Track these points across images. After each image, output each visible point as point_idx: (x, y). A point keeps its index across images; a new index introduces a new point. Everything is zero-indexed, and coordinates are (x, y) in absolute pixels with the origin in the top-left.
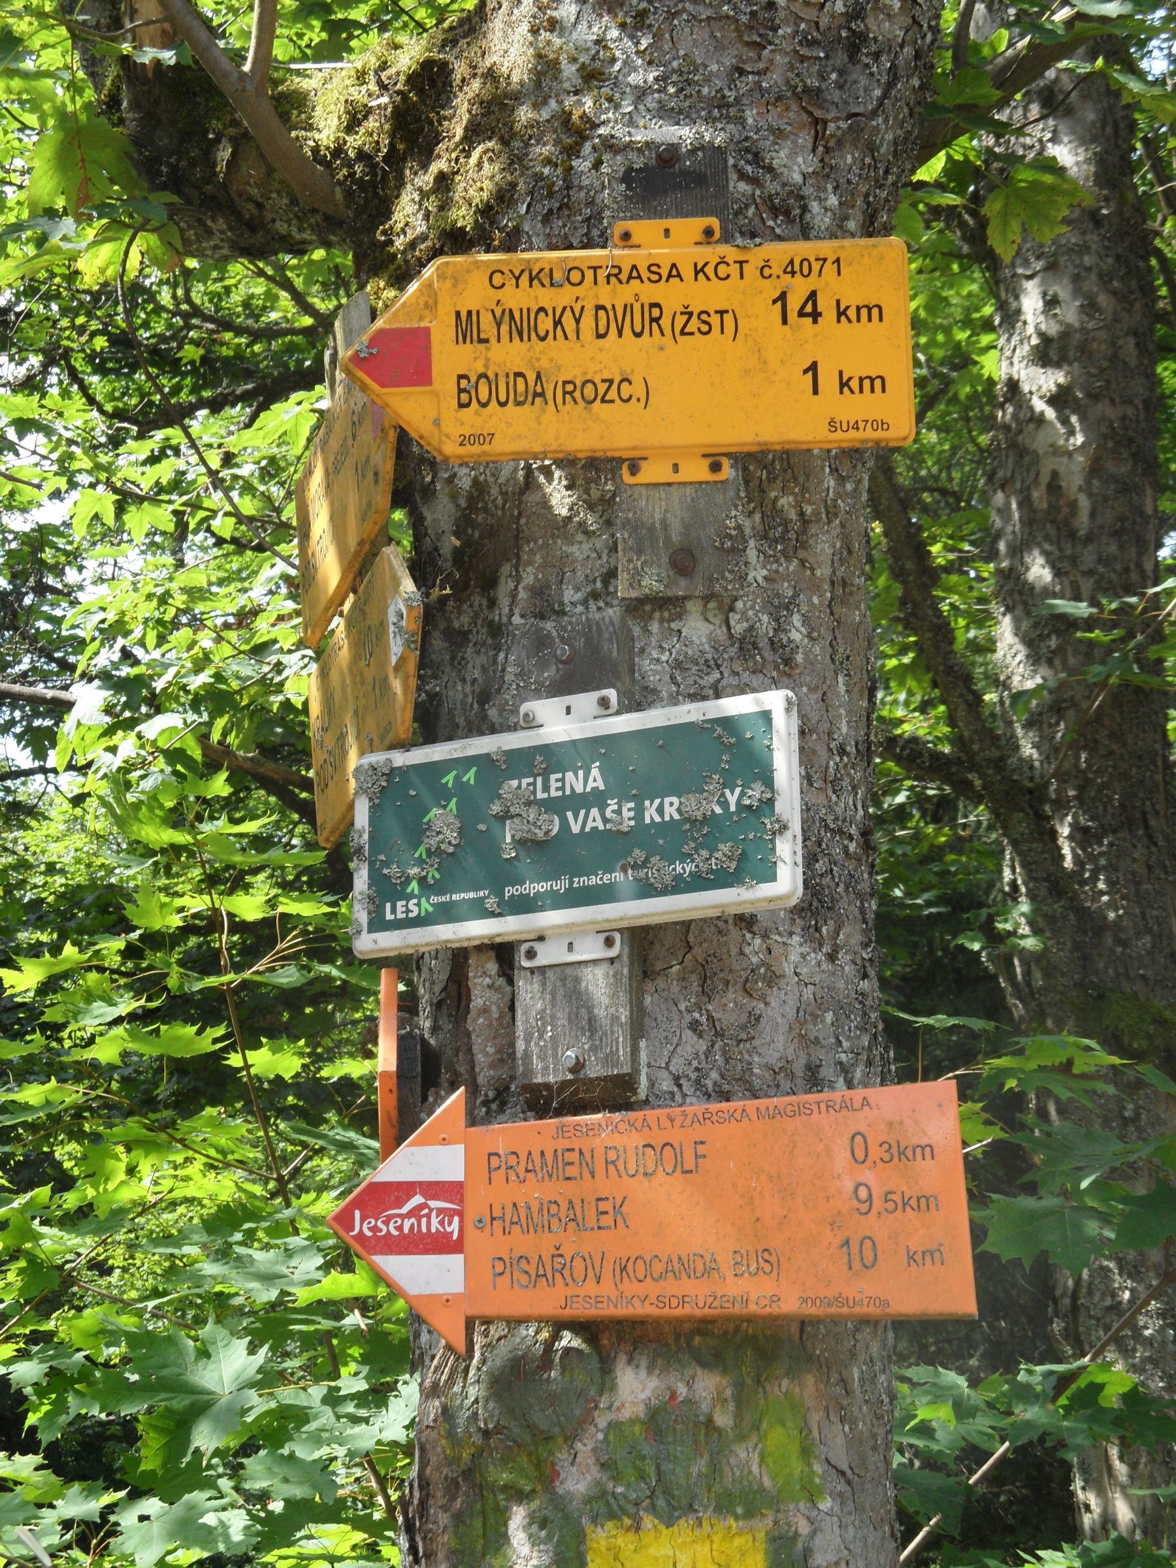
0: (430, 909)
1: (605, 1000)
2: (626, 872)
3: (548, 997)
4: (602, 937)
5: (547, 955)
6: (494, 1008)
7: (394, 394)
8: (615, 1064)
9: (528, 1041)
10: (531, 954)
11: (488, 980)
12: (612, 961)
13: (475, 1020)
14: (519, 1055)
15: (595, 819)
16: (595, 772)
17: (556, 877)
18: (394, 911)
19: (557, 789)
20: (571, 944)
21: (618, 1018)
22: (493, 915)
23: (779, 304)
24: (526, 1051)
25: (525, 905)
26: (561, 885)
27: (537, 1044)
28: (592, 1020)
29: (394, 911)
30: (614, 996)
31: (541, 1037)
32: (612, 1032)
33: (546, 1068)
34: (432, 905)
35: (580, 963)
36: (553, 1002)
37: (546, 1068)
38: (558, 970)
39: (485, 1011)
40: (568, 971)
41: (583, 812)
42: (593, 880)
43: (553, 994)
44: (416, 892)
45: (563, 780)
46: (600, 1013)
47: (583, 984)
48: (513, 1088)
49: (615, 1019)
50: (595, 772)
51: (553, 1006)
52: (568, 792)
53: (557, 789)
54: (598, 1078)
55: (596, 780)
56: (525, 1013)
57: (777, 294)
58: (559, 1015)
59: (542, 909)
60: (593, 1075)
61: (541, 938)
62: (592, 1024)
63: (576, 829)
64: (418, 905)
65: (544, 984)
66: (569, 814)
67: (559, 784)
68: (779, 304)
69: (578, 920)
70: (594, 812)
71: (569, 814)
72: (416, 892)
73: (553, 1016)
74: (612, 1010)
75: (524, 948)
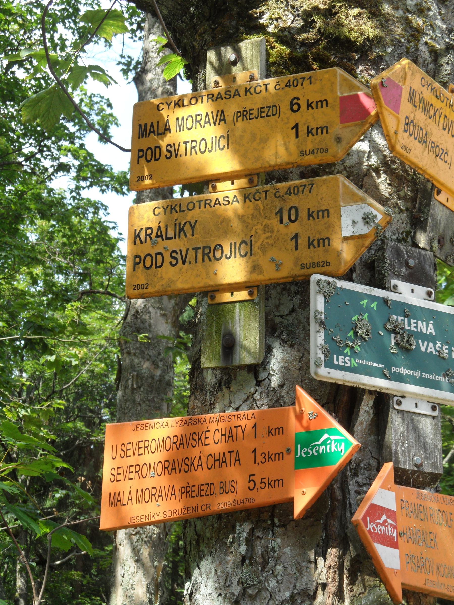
0: (356, 365)
1: (431, 436)
2: (445, 378)
3: (405, 426)
4: (431, 405)
5: (407, 405)
6: (365, 423)
7: (387, 110)
8: (436, 468)
9: (397, 446)
10: (399, 403)
11: (367, 409)
12: (434, 417)
13: (357, 427)
14: (393, 451)
15: (431, 349)
16: (431, 326)
17: (415, 369)
18: (338, 360)
19: (415, 327)
20: (416, 404)
21: (437, 446)
22: (388, 378)
23: (295, 129)
24: (396, 450)
25: (399, 378)
26: (417, 374)
27: (401, 448)
28: (425, 444)
29: (338, 360)
30: (435, 434)
31: (402, 446)
32: (435, 452)
33: (405, 461)
34: (357, 363)
35: (420, 414)
36: (408, 429)
37: (405, 461)
38: (410, 414)
39: (362, 423)
40: (414, 417)
41: (426, 343)
42: (431, 377)
43: (408, 425)
44: (349, 354)
45: (416, 323)
46: (429, 441)
47: (421, 425)
48: (362, 465)
49: (436, 446)
50: (431, 326)
51: (408, 432)
52: (419, 331)
53: (415, 327)
54: (428, 473)
55: (431, 330)
56: (395, 431)
57: (294, 124)
58: (410, 437)
59: (409, 383)
60: (426, 471)
61: (404, 397)
62: (425, 446)
63: (423, 350)
64: (350, 361)
65: (403, 419)
66: (420, 341)
67: (415, 325)
68: (295, 129)
69: (425, 394)
70: (431, 344)
71: (420, 341)
72: (349, 354)
73: (408, 437)
74: (434, 441)
75: (396, 399)
